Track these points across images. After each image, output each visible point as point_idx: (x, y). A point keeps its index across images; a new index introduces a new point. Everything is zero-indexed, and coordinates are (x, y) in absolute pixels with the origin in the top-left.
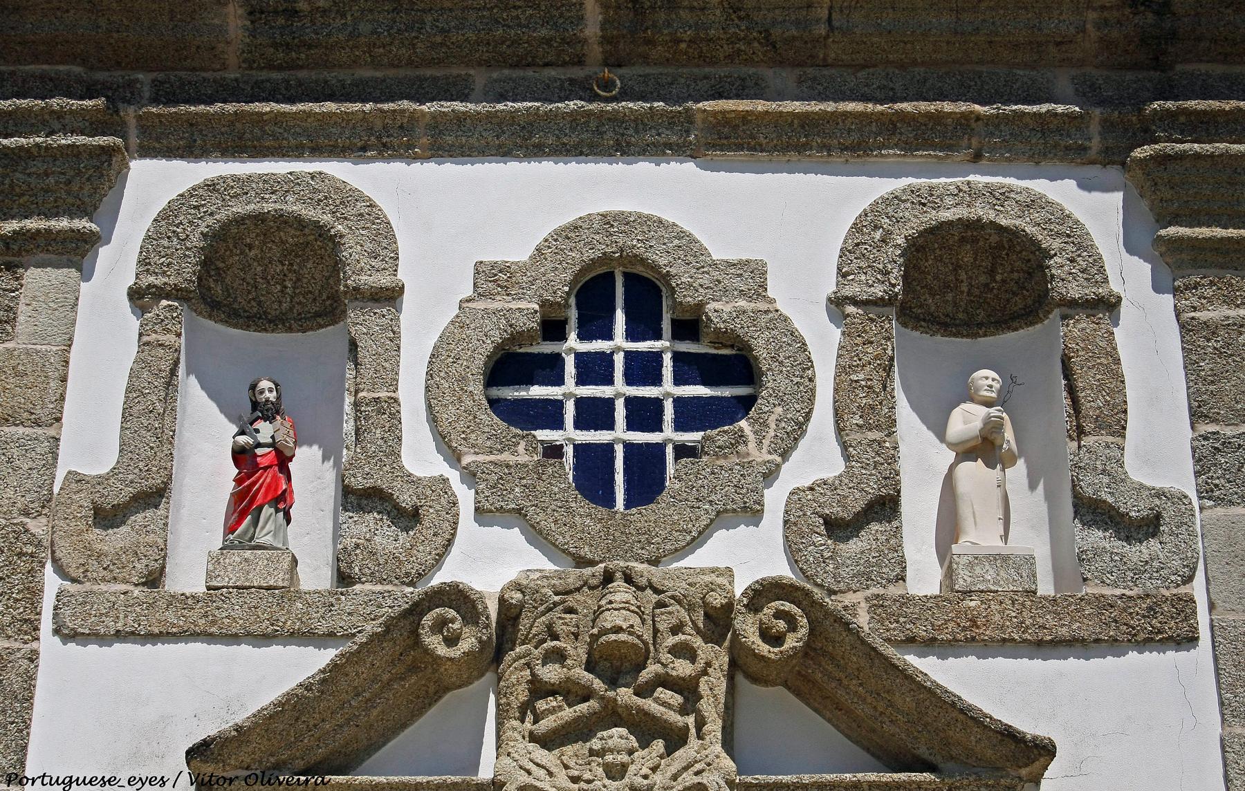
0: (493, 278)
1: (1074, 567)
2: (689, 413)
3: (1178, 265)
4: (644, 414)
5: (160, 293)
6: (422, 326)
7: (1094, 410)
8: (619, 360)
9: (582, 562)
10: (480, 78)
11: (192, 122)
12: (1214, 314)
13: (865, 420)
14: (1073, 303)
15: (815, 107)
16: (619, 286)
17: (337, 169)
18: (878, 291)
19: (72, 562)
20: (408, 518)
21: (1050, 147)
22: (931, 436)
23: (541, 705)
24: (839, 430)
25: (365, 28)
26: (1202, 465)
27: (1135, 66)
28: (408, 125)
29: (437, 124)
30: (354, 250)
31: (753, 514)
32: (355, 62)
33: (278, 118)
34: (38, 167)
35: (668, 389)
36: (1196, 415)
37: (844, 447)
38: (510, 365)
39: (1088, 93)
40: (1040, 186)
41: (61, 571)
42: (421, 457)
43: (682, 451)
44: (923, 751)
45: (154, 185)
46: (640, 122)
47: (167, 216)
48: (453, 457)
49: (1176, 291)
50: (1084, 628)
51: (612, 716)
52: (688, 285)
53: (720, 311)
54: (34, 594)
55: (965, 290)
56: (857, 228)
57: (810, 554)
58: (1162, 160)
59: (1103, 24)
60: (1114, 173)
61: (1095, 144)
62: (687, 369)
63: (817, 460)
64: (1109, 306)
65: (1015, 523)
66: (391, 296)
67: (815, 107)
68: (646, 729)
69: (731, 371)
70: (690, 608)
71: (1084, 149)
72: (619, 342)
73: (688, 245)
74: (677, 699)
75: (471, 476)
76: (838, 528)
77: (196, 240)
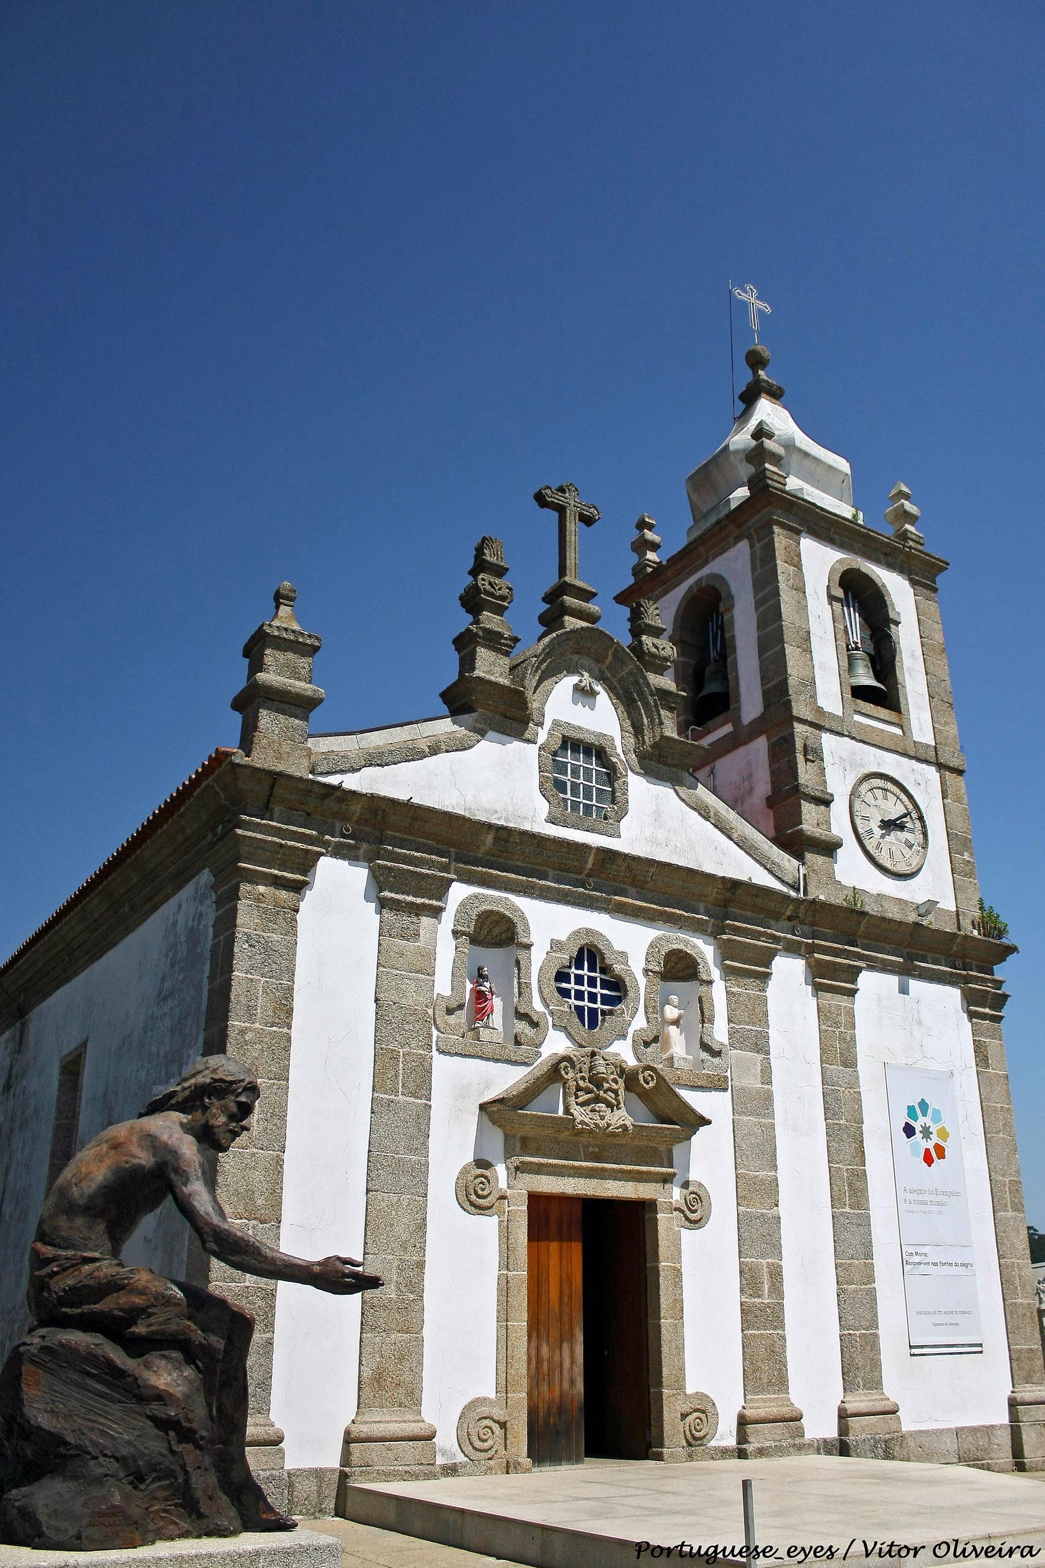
0: (556, 945)
2: (606, 1000)
3: (729, 973)
4: (593, 998)
5: (463, 933)
6: (537, 957)
7: (706, 1018)
8: (572, 976)
9: (581, 1046)
10: (551, 873)
11: (470, 872)
12: (735, 989)
13: (654, 1010)
14: (704, 981)
15: (643, 904)
17: (512, 897)
18: (657, 969)
19: (441, 1026)
20: (534, 1025)
21: (698, 928)
23: (579, 1093)
24: (646, 1013)
25: (527, 851)
26: (731, 1035)
27: (719, 906)
28: (533, 886)
29: (543, 888)
30: (520, 929)
31: (624, 1036)
32: (518, 860)
33: (497, 876)
34: (430, 881)
35: (598, 990)
36: (730, 1021)
37: (648, 1018)
38: (562, 976)
40: (695, 940)
41: (438, 1029)
42: (538, 1005)
43: (603, 1013)
44: (675, 1119)
45: (459, 892)
46: (598, 899)
47: (463, 904)
48: (547, 1006)
49: (726, 981)
50: (704, 1083)
51: (597, 1100)
53: (618, 968)
54: (430, 1036)
56: (651, 946)
57: (639, 1052)
58: (729, 940)
59: (717, 893)
60: (711, 939)
61: (710, 930)
62: (605, 985)
64: (710, 983)
66: (528, 947)
67: (643, 904)
68: (609, 1105)
69: (617, 988)
70: (616, 1067)
72: (585, 972)
73: (609, 944)
74: (613, 1096)
75: (552, 1013)
76: (647, 1044)
77: (474, 917)
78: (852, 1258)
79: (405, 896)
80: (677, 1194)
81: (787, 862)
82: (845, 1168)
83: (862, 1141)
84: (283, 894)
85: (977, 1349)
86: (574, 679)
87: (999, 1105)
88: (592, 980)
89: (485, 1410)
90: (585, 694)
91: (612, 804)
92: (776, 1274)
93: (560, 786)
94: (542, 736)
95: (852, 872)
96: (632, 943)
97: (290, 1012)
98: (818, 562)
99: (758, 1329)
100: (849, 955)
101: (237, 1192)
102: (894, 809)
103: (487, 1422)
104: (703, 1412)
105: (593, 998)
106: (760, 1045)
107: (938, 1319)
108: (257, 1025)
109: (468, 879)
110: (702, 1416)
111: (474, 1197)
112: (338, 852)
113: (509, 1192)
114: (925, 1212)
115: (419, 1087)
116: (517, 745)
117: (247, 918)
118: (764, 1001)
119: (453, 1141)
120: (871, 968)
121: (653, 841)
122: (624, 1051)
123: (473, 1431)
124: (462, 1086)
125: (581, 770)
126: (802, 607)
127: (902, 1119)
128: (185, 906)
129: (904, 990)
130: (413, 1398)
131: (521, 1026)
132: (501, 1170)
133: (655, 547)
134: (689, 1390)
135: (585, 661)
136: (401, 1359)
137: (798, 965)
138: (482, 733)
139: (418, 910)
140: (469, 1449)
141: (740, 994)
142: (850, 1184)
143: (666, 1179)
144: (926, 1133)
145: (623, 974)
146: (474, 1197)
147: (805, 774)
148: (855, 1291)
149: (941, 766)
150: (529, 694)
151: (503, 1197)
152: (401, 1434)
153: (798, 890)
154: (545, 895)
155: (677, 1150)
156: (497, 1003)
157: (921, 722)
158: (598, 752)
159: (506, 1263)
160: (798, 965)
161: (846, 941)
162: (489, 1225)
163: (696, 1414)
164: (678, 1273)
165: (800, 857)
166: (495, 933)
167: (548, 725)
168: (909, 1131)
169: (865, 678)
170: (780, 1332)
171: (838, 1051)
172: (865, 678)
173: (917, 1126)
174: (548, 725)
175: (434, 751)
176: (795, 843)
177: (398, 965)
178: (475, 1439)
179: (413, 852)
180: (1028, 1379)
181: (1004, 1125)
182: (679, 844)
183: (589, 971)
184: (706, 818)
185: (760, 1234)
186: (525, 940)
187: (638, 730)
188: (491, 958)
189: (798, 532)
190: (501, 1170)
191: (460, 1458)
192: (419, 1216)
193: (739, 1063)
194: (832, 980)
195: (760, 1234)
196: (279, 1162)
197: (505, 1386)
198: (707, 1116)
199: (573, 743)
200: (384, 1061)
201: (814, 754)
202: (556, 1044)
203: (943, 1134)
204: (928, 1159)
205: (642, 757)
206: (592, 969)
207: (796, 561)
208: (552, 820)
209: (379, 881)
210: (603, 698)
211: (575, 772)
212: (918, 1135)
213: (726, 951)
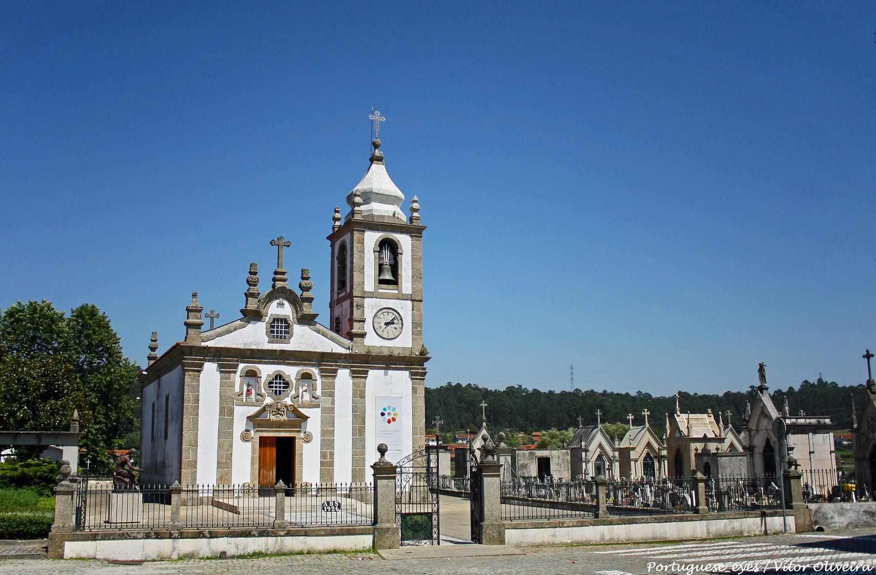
0: (269, 376)
1: (311, 401)
6: (263, 380)
13: (297, 389)
16: (279, 376)
21: (313, 365)
22: (849, 375)
38: (270, 383)
39: (317, 361)
42: (263, 391)
45: (241, 366)
52: (284, 377)
55: (307, 376)
63: (293, 392)
65: (307, 397)
69: (287, 384)
71: (67, 427)
79: (226, 369)
80: (302, 435)
81: (347, 342)
86: (277, 301)
88: (279, 383)
90: (281, 305)
92: (332, 454)
93: (273, 332)
94: (267, 319)
95: (372, 341)
96: (291, 372)
98: (372, 238)
100: (364, 367)
102: (389, 318)
106: (332, 395)
111: (245, 438)
112: (209, 361)
116: (260, 323)
117: (187, 380)
119: (239, 425)
122: (288, 401)
124: (242, 414)
125: (280, 328)
126: (362, 258)
128: (176, 372)
129: (386, 374)
131: (259, 397)
132: (252, 432)
133: (339, 219)
135: (281, 295)
137: (347, 372)
138: (249, 322)
139: (230, 372)
143: (299, 431)
146: (245, 438)
147: (357, 314)
149: (413, 301)
150: (262, 310)
153: (349, 349)
154: (265, 363)
155: (303, 424)
156: (253, 391)
157: (406, 285)
158: (284, 320)
159: (253, 453)
160: (347, 372)
161: (362, 363)
162: (249, 444)
165: (352, 340)
166: (252, 374)
168: (383, 414)
169: (388, 276)
171: (359, 394)
172: (388, 276)
175: (235, 330)
176: (351, 336)
177: (225, 385)
179: (227, 358)
185: (328, 444)
187: (297, 311)
188: (252, 380)
189: (364, 231)
190: (252, 432)
193: (325, 402)
194: (359, 374)
195: (328, 444)
196: (197, 434)
197: (253, 480)
200: (222, 410)
201: (361, 306)
202: (268, 400)
203: (396, 414)
204: (389, 422)
205: (298, 320)
207: (362, 242)
209: (220, 366)
210: (286, 303)
211: (278, 327)
213: (322, 371)
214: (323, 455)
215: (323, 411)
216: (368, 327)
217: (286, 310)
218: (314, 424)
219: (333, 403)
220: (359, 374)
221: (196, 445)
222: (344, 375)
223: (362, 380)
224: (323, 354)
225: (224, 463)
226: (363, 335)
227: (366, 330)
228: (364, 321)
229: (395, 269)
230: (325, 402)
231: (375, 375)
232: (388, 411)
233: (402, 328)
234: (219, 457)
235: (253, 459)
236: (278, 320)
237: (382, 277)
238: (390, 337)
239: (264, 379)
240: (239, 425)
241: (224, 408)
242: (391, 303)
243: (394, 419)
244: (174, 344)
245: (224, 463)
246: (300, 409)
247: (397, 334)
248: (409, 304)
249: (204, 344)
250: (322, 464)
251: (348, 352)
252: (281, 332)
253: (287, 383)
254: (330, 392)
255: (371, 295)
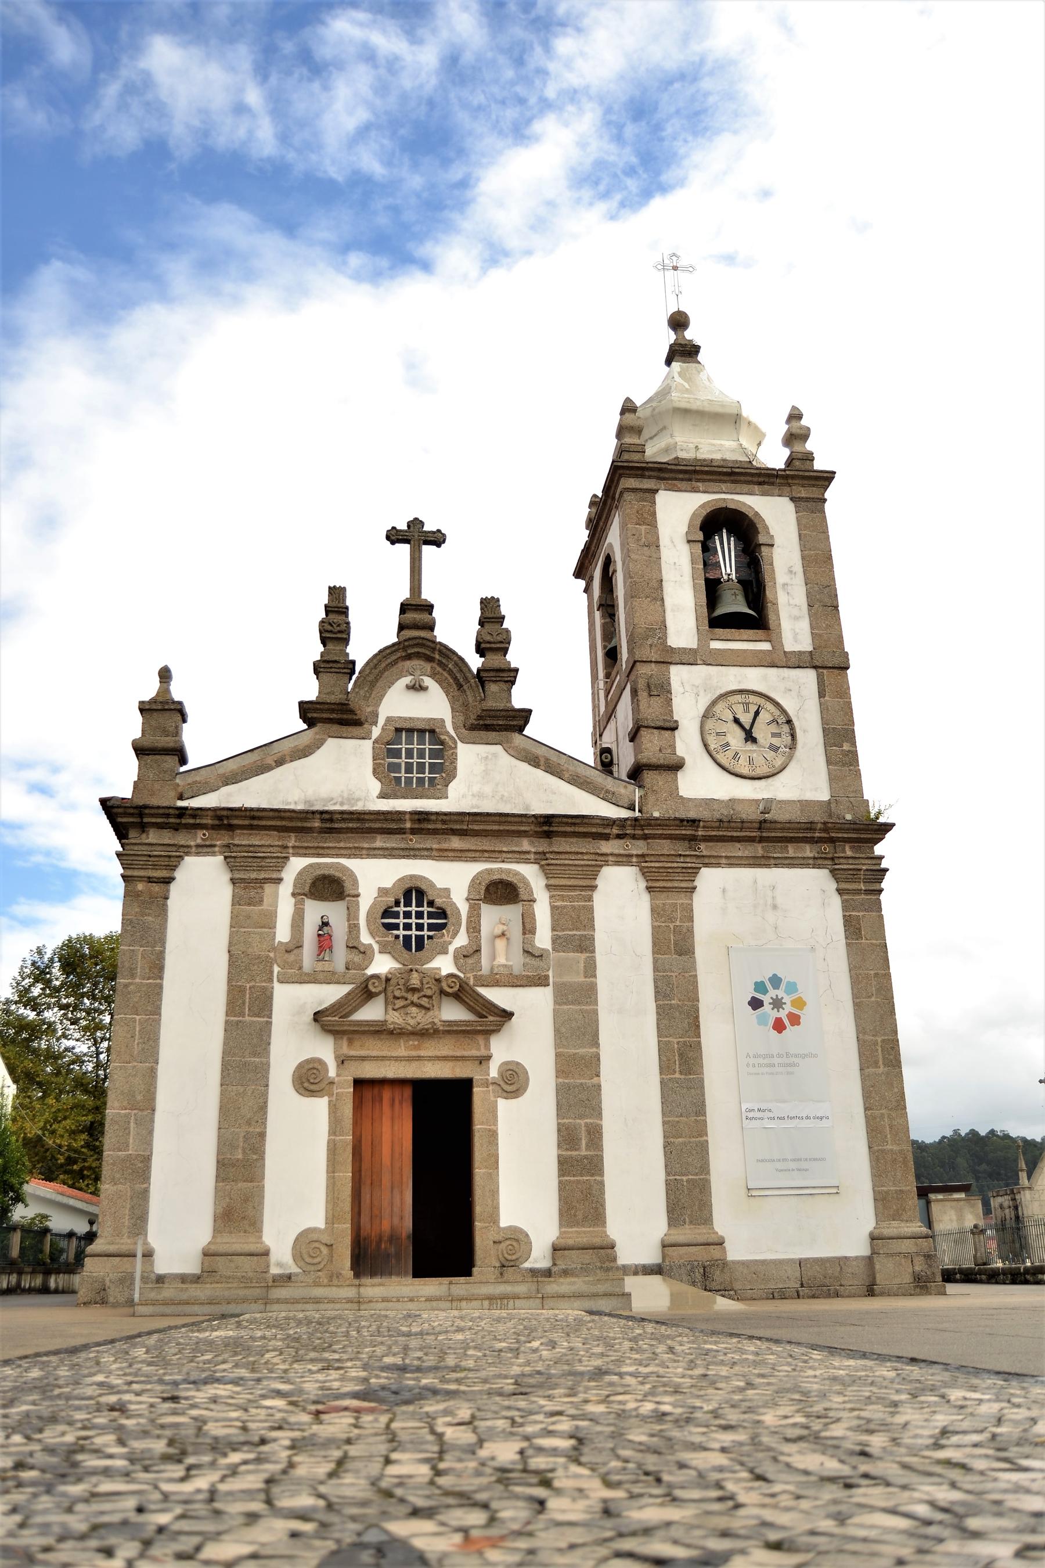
0: (383, 892)
2: (431, 927)
4: (420, 927)
6: (365, 903)
7: (528, 928)
16: (414, 892)
21: (522, 857)
35: (426, 921)
38: (387, 913)
42: (365, 938)
43: (430, 937)
52: (431, 895)
54: (272, 972)
55: (502, 891)
63: (461, 940)
72: (413, 909)
73: (432, 885)
78: (681, 1116)
82: (675, 1041)
83: (697, 1017)
84: (156, 888)
85: (836, 1191)
87: (872, 972)
88: (415, 915)
89: (315, 1237)
90: (417, 687)
91: (442, 771)
94: (376, 732)
96: (453, 878)
97: (161, 968)
99: (574, 1176)
101: (122, 1093)
103: (317, 1245)
104: (517, 1240)
105: (420, 927)
106: (586, 945)
107: (779, 1165)
108: (137, 980)
109: (302, 851)
110: (514, 1244)
113: (336, 1079)
114: (772, 1074)
115: (262, 1010)
118: (591, 910)
120: (707, 865)
121: (480, 795)
122: (444, 965)
123: (304, 1251)
125: (411, 757)
127: (750, 993)
130: (255, 1225)
134: (504, 1223)
136: (246, 1200)
140: (302, 1264)
141: (565, 907)
142: (681, 1055)
144: (777, 1004)
145: (443, 906)
146: (309, 1079)
148: (684, 1143)
149: (815, 667)
151: (332, 1083)
152: (243, 1251)
153: (631, 808)
158: (430, 731)
159: (334, 1128)
162: (320, 1106)
163: (508, 1242)
164: (493, 1135)
166: (329, 887)
167: (381, 721)
169: (734, 603)
170: (598, 1178)
173: (766, 999)
174: (381, 721)
178: (305, 1256)
180: (896, 1216)
181: (878, 990)
182: (506, 794)
183: (417, 906)
184: (537, 765)
186: (352, 892)
191: (294, 1269)
192: (261, 1100)
194: (669, 888)
197: (332, 1218)
198: (508, 1008)
199: (403, 730)
202: (382, 965)
203: (800, 1003)
206: (419, 904)
208: (383, 796)
210: (428, 681)
211: (409, 753)
212: (767, 1007)
214: (567, 1137)
215: (562, 996)
216: (687, 743)
217: (434, 704)
218: (529, 1037)
219: (591, 969)
220: (669, 888)
221: (148, 1105)
222: (621, 897)
223: (681, 900)
224: (548, 820)
225: (240, 1165)
226: (676, 766)
227: (681, 751)
228: (772, 545)
229: (754, 584)
230: (564, 968)
231: (721, 892)
232: (772, 993)
233: (793, 746)
234: (224, 1144)
235: (333, 1150)
236: (410, 731)
237: (720, 611)
238: (759, 772)
239: (367, 900)
240: (292, 1040)
241: (242, 990)
242: (753, 678)
243: (795, 1019)
244: (763, 429)
245: (240, 1165)
246: (483, 991)
247: (778, 763)
248: (808, 678)
249: (181, 804)
250: (565, 1166)
251: (624, 814)
252: (421, 767)
253: (442, 914)
254: (577, 933)
255: (689, 658)
